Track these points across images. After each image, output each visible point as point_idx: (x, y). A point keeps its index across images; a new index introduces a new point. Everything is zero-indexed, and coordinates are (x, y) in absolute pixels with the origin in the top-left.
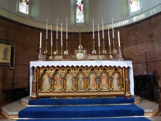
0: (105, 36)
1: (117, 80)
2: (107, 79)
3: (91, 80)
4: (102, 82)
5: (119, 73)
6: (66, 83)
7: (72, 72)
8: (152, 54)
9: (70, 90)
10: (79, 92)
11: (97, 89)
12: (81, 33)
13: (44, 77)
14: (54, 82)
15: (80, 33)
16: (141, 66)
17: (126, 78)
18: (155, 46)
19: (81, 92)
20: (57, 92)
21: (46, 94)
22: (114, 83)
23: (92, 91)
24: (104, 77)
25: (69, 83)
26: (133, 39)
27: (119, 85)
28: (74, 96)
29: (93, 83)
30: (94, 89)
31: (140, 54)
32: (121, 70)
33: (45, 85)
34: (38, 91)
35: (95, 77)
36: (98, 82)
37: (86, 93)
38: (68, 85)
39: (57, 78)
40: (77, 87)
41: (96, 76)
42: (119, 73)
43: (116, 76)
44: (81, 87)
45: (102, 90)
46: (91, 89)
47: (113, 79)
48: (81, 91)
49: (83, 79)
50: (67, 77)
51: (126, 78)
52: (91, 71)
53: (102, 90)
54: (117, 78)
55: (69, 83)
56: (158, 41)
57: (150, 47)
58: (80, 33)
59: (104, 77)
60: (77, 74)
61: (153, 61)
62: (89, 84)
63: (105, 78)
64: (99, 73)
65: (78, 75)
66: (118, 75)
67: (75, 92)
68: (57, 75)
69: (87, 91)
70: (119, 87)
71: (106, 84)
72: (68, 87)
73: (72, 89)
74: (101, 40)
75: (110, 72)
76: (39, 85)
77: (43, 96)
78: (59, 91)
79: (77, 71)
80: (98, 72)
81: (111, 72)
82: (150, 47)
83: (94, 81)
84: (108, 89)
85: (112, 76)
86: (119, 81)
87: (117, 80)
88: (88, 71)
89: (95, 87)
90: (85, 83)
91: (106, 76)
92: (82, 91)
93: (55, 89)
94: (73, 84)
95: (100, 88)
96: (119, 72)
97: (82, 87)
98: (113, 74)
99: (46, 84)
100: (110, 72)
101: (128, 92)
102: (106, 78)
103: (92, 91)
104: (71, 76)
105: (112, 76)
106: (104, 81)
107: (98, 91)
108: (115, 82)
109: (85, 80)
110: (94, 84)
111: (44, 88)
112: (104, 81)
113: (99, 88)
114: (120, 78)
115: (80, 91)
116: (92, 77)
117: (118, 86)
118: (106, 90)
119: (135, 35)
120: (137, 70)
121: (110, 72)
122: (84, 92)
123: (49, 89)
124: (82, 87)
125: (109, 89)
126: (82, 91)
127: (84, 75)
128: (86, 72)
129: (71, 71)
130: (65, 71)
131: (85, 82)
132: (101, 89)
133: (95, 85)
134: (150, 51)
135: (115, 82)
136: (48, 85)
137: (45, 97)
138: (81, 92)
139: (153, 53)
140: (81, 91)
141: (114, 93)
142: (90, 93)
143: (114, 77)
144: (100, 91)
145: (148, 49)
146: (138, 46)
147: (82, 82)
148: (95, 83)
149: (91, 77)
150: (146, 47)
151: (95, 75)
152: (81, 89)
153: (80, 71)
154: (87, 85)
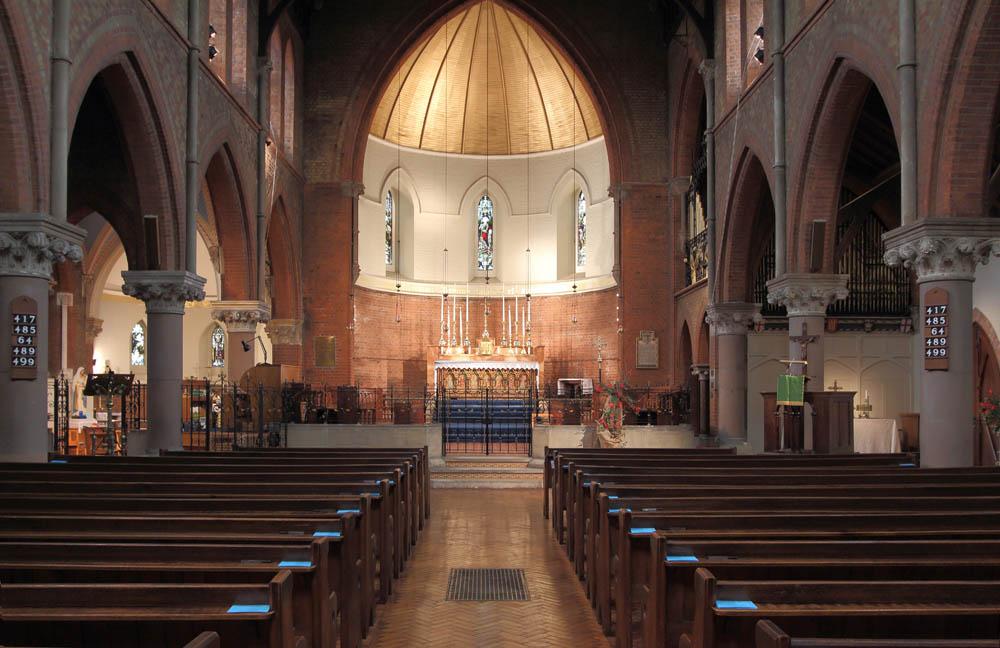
55: (474, 384)
116: (499, 378)
121: (517, 375)
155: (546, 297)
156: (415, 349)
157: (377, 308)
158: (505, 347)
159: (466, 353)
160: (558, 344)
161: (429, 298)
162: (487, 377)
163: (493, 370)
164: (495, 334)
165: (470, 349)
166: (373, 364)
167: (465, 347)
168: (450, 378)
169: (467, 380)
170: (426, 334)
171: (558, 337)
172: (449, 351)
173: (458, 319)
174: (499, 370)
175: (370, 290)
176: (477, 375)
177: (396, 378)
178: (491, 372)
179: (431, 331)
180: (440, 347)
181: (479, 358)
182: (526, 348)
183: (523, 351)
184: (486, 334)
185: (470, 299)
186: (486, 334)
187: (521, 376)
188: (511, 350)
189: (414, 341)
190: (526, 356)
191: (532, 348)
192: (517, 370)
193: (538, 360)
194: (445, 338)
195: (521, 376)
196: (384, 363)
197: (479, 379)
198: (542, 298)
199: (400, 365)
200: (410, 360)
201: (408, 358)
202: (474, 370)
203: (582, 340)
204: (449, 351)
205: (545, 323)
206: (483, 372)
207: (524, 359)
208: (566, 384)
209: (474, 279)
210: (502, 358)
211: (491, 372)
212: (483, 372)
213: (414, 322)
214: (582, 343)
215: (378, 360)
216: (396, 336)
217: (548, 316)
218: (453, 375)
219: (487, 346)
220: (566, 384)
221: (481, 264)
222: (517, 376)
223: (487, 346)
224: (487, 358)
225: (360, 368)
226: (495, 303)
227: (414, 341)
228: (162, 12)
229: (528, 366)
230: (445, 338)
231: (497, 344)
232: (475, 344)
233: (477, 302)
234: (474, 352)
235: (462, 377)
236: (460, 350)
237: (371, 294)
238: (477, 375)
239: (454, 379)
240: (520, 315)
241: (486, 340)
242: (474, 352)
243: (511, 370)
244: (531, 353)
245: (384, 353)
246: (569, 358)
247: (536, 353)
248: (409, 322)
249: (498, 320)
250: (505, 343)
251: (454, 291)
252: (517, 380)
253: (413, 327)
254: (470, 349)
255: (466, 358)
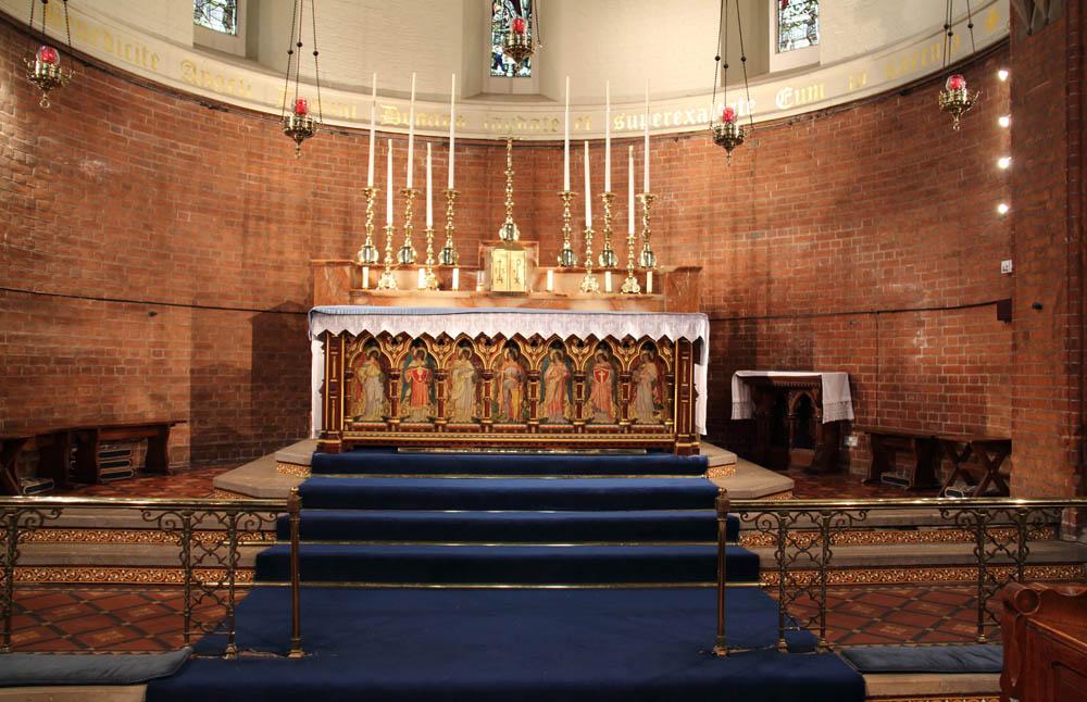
0: (543, 174)
1: (653, 389)
2: (614, 384)
3: (551, 386)
4: (592, 396)
5: (659, 362)
6: (449, 397)
7: (429, 354)
8: (841, 280)
9: (468, 422)
10: (500, 431)
11: (571, 422)
12: (517, 144)
13: (364, 369)
14: (404, 391)
15: (509, 146)
16: (794, 329)
17: (685, 380)
18: (855, 242)
19: (510, 431)
20: (416, 430)
21: (375, 434)
22: (638, 401)
23: (552, 426)
24: (602, 374)
25: (461, 392)
26: (767, 195)
27: (658, 407)
28: (483, 445)
29: (558, 398)
30: (562, 421)
31: (791, 275)
32: (667, 352)
33: (367, 402)
34: (345, 423)
35: (565, 374)
36: (575, 395)
37: (530, 435)
38: (457, 403)
39: (415, 373)
40: (496, 411)
41: (570, 370)
42: (659, 362)
43: (651, 370)
44: (511, 414)
45: (592, 426)
46: (547, 419)
47: (635, 384)
48: (510, 426)
49: (520, 381)
50: (456, 372)
51: (685, 380)
52: (549, 352)
53: (592, 426)
54: (652, 383)
55: (461, 392)
56: (866, 224)
57: (834, 244)
58: (509, 146)
59: (602, 374)
60: (542, 360)
61: (839, 314)
62: (542, 400)
63: (605, 377)
64: (580, 358)
65: (500, 366)
66: (659, 369)
67: (487, 429)
68: (414, 362)
69: (533, 429)
70: (659, 416)
71: (609, 405)
72: (459, 412)
73: (473, 418)
74: (401, 194)
75: (623, 356)
76: (673, 397)
77: (387, 444)
78: (422, 425)
79: (589, 351)
80: (577, 356)
81: (630, 356)
82: (838, 244)
83: (560, 390)
84: (614, 421)
85: (631, 373)
86: (660, 390)
87: (653, 389)
88: (400, 348)
89: (563, 413)
90: (526, 398)
91: (611, 372)
92: (515, 426)
93: (408, 417)
94: (479, 400)
95: (584, 417)
96: (662, 361)
97: (515, 414)
98: (545, 362)
99: (371, 398)
100: (623, 356)
101: (687, 432)
102: (609, 381)
103: (552, 426)
104: (470, 366)
105: (635, 372)
106: (601, 390)
107: (576, 428)
108: (645, 394)
109: (525, 385)
110: (563, 402)
111: (365, 414)
112: (601, 390)
113: (579, 416)
114: (664, 380)
115: (505, 426)
116: (555, 372)
117: (655, 414)
118: (607, 426)
119: (777, 178)
120: (777, 351)
121: (626, 359)
122: (521, 431)
123: (383, 417)
124: (515, 414)
125: (386, 419)
126: (515, 426)
127: (524, 367)
128: (531, 355)
129: (426, 347)
130: (448, 347)
131: (526, 393)
132: (634, 422)
133: (563, 408)
134: (833, 266)
135: (645, 394)
136: (378, 400)
137: (371, 444)
138: (510, 431)
139: (846, 276)
140: (510, 426)
141: (356, 433)
142: (543, 435)
143: (642, 376)
144: (583, 427)
145: (828, 253)
146: (788, 236)
147: (515, 393)
148: (566, 397)
149: (548, 373)
150: (820, 242)
151: (565, 368)
152: (511, 421)
153: (507, 350)
154: (533, 404)
155: (688, 136)
156: (293, 277)
157: (152, 140)
158: (569, 270)
159: (445, 286)
160: (724, 269)
161: (344, 131)
162: (511, 368)
163: (535, 341)
164: (540, 229)
165: (456, 273)
166: (129, 319)
167: (444, 271)
168: (371, 372)
169: (436, 377)
170: (331, 237)
171: (724, 248)
172: (390, 280)
173: (420, 173)
174: (556, 342)
175: (129, 78)
176: (476, 360)
177: (225, 366)
178: (480, 350)
179: (347, 229)
180: (360, 269)
181: (486, 305)
182: (640, 275)
183: (632, 284)
184: (509, 230)
185: (462, 144)
186: (509, 230)
187: (637, 365)
188: (589, 281)
189: (292, 255)
190: (641, 299)
191: (656, 277)
192: (628, 342)
193: (679, 307)
194: (380, 242)
195: (637, 365)
196: (184, 318)
197: (482, 377)
198: (677, 138)
199: (243, 327)
200: (277, 312)
201: (269, 306)
202: (464, 341)
203: (805, 255)
204: (390, 280)
205: (682, 210)
206: (499, 350)
207: (633, 307)
208: (757, 387)
209: (476, 93)
210: (561, 302)
211: (526, 350)
212: (499, 350)
213: (295, 197)
214: (811, 264)
215: (152, 308)
216: (229, 237)
217: (709, 170)
218: (383, 361)
219: (510, 265)
220: (757, 387)
221: (498, 61)
222: (626, 363)
223: (510, 265)
224: (521, 301)
225: (54, 331)
226: (539, 156)
227: (292, 255)
228: (905, 693)
229: (669, 328)
230: (380, 242)
231: (547, 261)
232: (476, 263)
233: (483, 154)
234: (469, 284)
235: (419, 367)
236: (424, 278)
237: (125, 90)
238: (476, 360)
239: (388, 376)
240: (620, 185)
241: (509, 245)
242: (469, 284)
243: (604, 344)
244: (656, 290)
245: (179, 286)
246: (761, 310)
247: (673, 290)
248: (275, 197)
249: (547, 202)
250: (573, 260)
251: (407, 118)
252: (624, 383)
253: (289, 213)
254: (456, 273)
255: (443, 300)
